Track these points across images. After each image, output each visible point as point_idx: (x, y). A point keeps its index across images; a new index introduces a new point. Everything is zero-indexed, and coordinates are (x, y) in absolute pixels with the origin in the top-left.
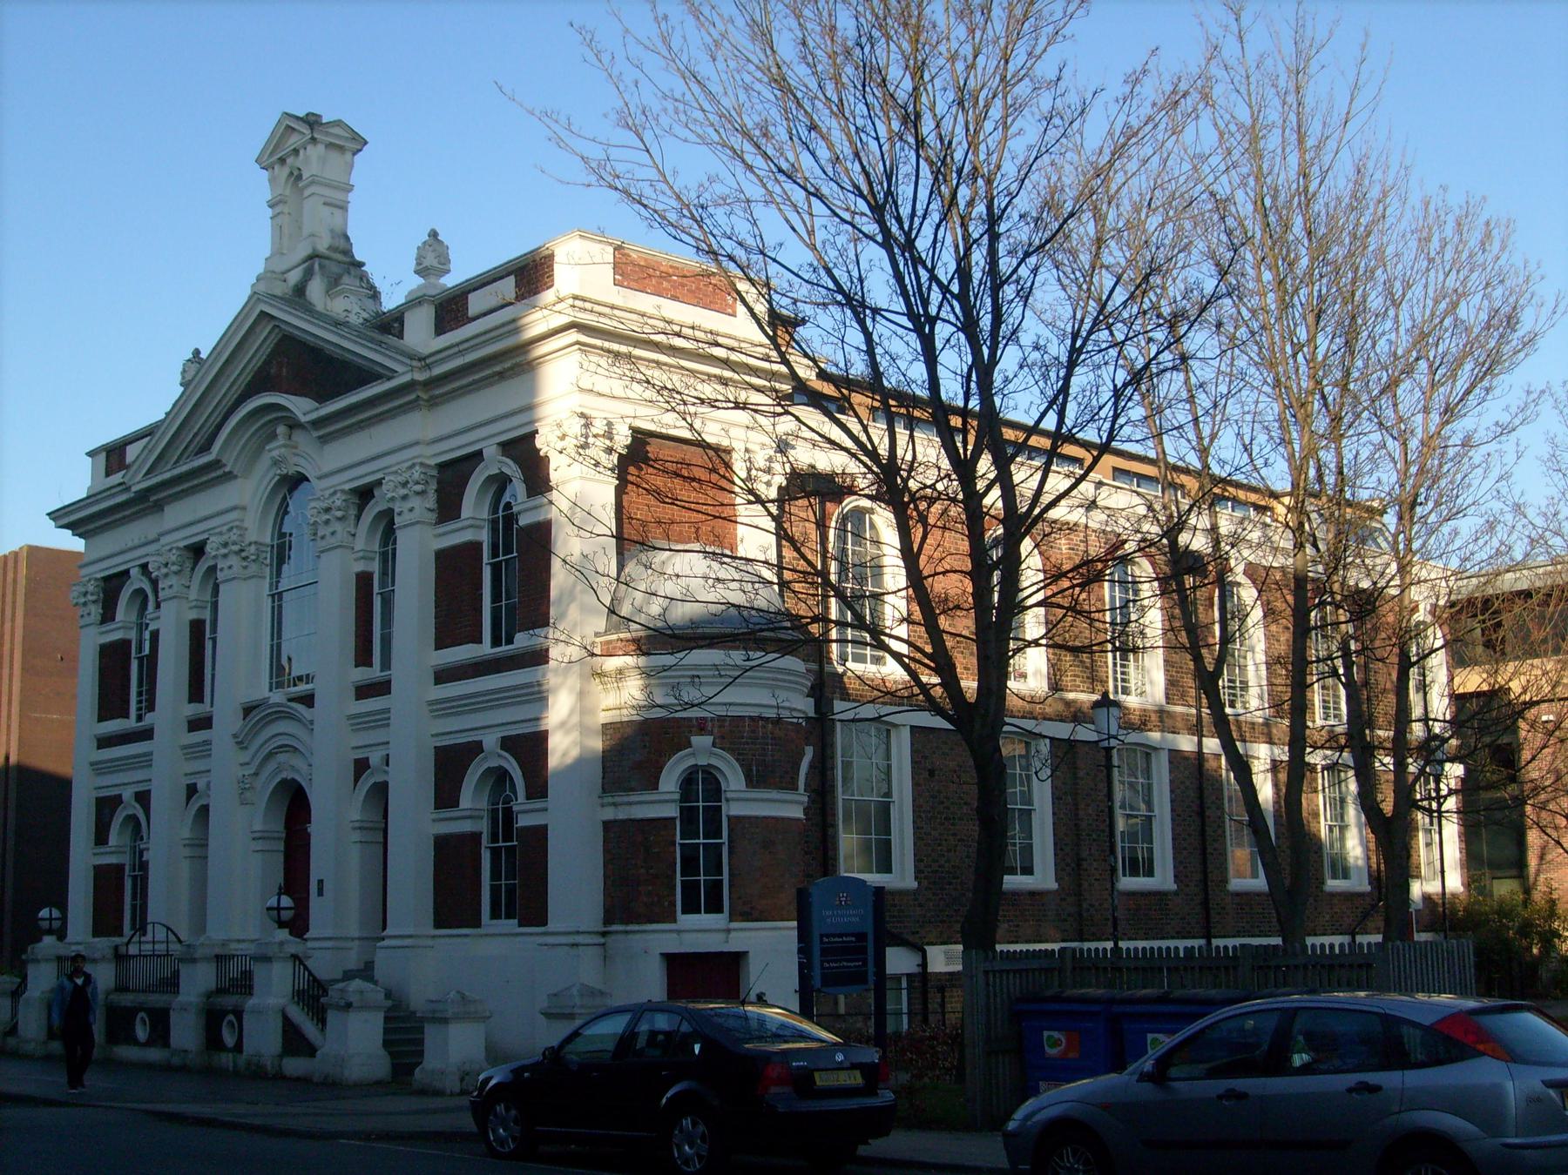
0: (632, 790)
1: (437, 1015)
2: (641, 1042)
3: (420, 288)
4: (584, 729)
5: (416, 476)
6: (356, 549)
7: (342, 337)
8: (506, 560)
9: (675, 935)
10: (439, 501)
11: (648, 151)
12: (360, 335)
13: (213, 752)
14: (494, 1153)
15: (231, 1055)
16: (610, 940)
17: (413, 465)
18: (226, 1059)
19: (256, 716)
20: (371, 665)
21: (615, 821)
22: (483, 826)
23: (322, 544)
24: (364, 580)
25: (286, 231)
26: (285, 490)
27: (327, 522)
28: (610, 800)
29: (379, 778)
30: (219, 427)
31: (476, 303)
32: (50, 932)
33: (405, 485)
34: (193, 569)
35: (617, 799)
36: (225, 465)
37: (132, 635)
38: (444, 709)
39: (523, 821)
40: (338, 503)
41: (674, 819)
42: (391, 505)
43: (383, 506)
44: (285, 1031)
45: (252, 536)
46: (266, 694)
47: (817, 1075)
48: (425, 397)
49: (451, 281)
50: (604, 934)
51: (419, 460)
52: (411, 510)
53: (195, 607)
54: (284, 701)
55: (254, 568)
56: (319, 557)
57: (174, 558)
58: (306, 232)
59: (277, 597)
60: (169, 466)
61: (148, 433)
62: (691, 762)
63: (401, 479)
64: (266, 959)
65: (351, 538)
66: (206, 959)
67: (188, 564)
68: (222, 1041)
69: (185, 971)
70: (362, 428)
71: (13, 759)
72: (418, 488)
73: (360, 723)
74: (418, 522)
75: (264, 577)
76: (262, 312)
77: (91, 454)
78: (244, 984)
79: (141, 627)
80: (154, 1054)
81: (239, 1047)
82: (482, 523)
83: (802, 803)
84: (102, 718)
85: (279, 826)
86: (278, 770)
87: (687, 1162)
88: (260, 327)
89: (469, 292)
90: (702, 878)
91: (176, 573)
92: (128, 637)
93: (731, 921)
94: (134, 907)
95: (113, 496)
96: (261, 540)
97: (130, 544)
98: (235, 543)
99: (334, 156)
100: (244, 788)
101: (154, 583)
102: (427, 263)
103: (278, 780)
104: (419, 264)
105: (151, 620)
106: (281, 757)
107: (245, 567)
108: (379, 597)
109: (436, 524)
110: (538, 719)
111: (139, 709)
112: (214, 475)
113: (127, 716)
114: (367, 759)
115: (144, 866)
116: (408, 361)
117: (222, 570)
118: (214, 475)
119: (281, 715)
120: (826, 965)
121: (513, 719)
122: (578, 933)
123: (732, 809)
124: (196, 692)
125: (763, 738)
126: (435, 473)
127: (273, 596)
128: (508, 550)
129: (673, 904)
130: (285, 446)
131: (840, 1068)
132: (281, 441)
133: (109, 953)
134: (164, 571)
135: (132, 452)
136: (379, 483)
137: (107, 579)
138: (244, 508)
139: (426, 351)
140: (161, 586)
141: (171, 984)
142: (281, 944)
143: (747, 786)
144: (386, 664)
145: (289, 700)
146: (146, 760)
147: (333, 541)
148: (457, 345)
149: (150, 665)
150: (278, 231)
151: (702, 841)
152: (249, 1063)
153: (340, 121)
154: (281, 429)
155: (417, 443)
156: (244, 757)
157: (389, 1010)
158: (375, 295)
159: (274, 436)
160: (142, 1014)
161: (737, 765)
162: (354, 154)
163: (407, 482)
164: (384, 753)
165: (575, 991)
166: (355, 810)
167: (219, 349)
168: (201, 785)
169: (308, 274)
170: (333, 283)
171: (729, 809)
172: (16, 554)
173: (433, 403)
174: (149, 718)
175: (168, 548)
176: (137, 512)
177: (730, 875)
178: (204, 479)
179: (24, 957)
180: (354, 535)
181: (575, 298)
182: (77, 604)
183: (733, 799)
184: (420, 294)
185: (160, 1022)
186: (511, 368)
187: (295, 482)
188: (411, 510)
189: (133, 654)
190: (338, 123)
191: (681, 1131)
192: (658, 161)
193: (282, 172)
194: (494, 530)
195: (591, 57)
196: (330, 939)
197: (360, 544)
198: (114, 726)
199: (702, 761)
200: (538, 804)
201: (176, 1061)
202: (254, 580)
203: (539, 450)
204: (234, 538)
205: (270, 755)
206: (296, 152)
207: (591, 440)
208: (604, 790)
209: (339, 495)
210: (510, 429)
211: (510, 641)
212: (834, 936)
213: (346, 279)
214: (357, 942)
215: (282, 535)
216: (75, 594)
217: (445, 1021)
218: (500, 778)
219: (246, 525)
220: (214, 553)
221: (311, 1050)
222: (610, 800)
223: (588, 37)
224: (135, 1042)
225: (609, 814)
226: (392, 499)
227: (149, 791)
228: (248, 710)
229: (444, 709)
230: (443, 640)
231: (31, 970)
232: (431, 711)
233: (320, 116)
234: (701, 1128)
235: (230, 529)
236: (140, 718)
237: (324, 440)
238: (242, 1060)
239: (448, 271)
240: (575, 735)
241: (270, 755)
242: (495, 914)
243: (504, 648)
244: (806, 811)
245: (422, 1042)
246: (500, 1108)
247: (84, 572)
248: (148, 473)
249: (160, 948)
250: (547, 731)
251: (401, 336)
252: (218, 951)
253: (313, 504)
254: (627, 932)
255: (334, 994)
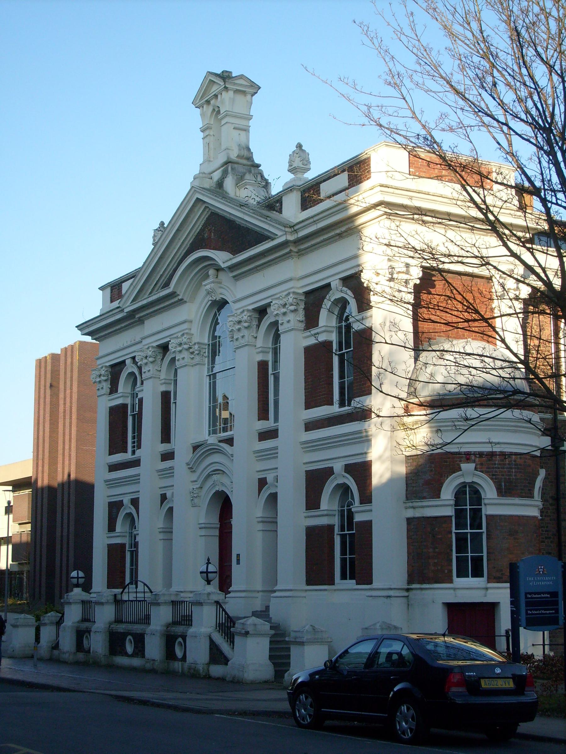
0: (424, 498)
1: (297, 640)
2: (382, 659)
3: (291, 181)
4: (393, 460)
5: (291, 300)
6: (258, 346)
7: (244, 213)
8: (347, 352)
9: (452, 591)
10: (306, 316)
11: (404, 99)
12: (255, 212)
13: (175, 474)
14: (300, 725)
15: (180, 663)
16: (411, 594)
17: (289, 294)
18: (177, 666)
19: (200, 451)
20: (267, 419)
21: (414, 518)
22: (335, 521)
23: (237, 344)
24: (263, 366)
25: (211, 146)
26: (215, 310)
27: (239, 330)
28: (411, 504)
29: (273, 491)
30: (175, 270)
31: (326, 188)
32: (77, 586)
33: (284, 305)
34: (162, 359)
35: (415, 504)
36: (178, 295)
37: (128, 401)
38: (312, 446)
39: (358, 518)
40: (245, 318)
41: (451, 517)
42: (277, 318)
43: (272, 320)
44: (211, 649)
45: (195, 339)
46: (207, 437)
47: (483, 682)
48: (295, 250)
49: (310, 175)
50: (408, 590)
51: (292, 290)
52: (289, 321)
53: (164, 383)
54: (216, 442)
55: (197, 359)
56: (235, 351)
57: (150, 353)
58: (223, 147)
59: (213, 377)
60: (146, 296)
61: (132, 276)
62: (461, 480)
63: (281, 302)
64: (200, 604)
65: (254, 340)
66: (165, 603)
67: (159, 357)
68: (175, 654)
69: (154, 612)
70: (259, 271)
71: (73, 476)
72: (292, 308)
73: (262, 455)
74: (292, 330)
75: (204, 365)
76: (197, 198)
77: (102, 288)
78: (187, 620)
79: (134, 396)
80: (136, 662)
81: (184, 658)
82: (268, 350)
83: (537, 506)
84: (308, 406)
85: (215, 520)
86: (214, 485)
87: (404, 733)
88: (197, 208)
89: (321, 182)
90: (470, 554)
91: (152, 362)
92: (125, 402)
93: (488, 583)
94: (131, 570)
95: (113, 315)
96: (202, 341)
97: (125, 345)
98: (185, 344)
99: (239, 98)
100: (194, 497)
101: (140, 368)
102: (295, 165)
103: (214, 491)
104: (290, 166)
105: (139, 391)
106: (215, 477)
107: (192, 359)
108: (272, 376)
109: (305, 330)
110: (366, 453)
111: (134, 447)
112: (173, 301)
113: (125, 451)
114: (266, 478)
115: (136, 545)
116: (283, 228)
117: (178, 360)
118: (173, 301)
119: (215, 451)
120: (529, 612)
121: (354, 453)
122: (391, 589)
123: (488, 510)
124: (166, 436)
125: (509, 464)
126: (303, 298)
127: (210, 376)
128: (348, 346)
129: (451, 571)
130: (213, 282)
131: (498, 677)
132: (211, 279)
133: (111, 598)
134: (145, 361)
135: (125, 286)
136: (269, 305)
137: (112, 366)
138: (191, 322)
139: (295, 221)
140: (143, 370)
141: (147, 619)
142: (209, 594)
143: (498, 496)
144: (276, 419)
145: (220, 441)
146: (136, 479)
147: (242, 342)
148: (312, 217)
149: (138, 419)
150: (207, 146)
151: (469, 531)
152: (190, 669)
153: (243, 75)
154: (211, 272)
155: (291, 280)
156: (194, 477)
157: (273, 636)
158: (266, 185)
159: (207, 276)
160: (130, 637)
161: (491, 482)
162: (252, 95)
163: (286, 304)
164: (275, 474)
165: (378, 626)
166: (259, 512)
167: (173, 222)
168: (168, 495)
169: (225, 174)
170: (240, 179)
171: (486, 510)
172: (72, 347)
173: (301, 253)
174: (138, 452)
175: (147, 347)
176: (130, 324)
177: (488, 553)
178: (162, 305)
179: (62, 601)
180: (256, 338)
181: (382, 186)
182: (95, 382)
183: (489, 504)
184: (291, 185)
185: (139, 640)
186: (345, 231)
187: (221, 304)
188: (289, 321)
189: (129, 413)
190: (242, 77)
191: (401, 713)
192: (411, 105)
193: (208, 110)
194: (340, 333)
195: (367, 41)
196: (244, 591)
197: (260, 343)
198: (119, 457)
199: (468, 480)
200: (366, 507)
201: (148, 666)
202: (198, 366)
203: (363, 283)
204: (185, 340)
205: (209, 476)
206: (216, 96)
207: (395, 276)
208: (407, 499)
209: (245, 313)
210: (346, 270)
211: (349, 405)
212: (535, 593)
213: (247, 176)
214: (261, 594)
215: (214, 337)
216: (94, 376)
217: (302, 644)
218: (345, 489)
219: (192, 332)
220: (173, 350)
221: (225, 661)
222: (411, 504)
223: (366, 28)
224: (126, 654)
225: (410, 514)
226: (277, 315)
227: (139, 498)
228: (195, 448)
229: (312, 446)
230: (112, 451)
231: (67, 609)
232: (303, 448)
233: (231, 72)
234: (412, 712)
235: (183, 335)
236: (134, 453)
237: (237, 278)
238: (186, 665)
239: (309, 169)
240: (387, 464)
241: (209, 476)
242: (343, 577)
243: (346, 408)
244: (542, 512)
245: (289, 657)
246: (302, 697)
247: (99, 362)
248: (134, 300)
249: (140, 595)
250: (371, 461)
251: (280, 211)
252: (173, 598)
253: (231, 319)
254: (421, 589)
255: (238, 626)
